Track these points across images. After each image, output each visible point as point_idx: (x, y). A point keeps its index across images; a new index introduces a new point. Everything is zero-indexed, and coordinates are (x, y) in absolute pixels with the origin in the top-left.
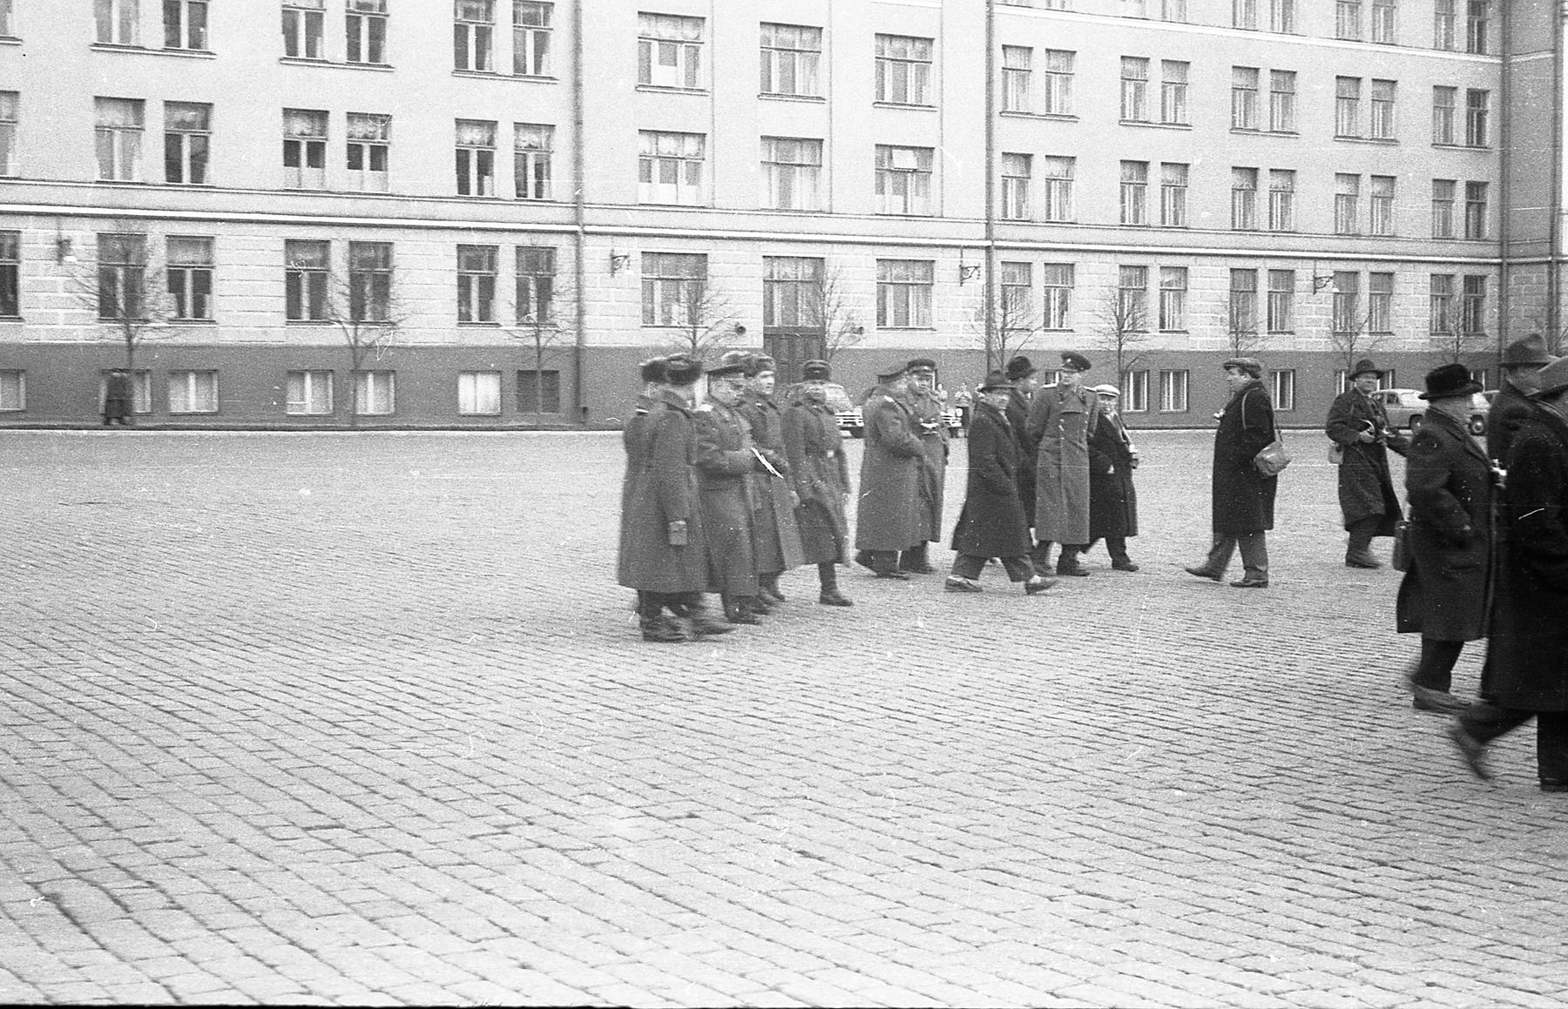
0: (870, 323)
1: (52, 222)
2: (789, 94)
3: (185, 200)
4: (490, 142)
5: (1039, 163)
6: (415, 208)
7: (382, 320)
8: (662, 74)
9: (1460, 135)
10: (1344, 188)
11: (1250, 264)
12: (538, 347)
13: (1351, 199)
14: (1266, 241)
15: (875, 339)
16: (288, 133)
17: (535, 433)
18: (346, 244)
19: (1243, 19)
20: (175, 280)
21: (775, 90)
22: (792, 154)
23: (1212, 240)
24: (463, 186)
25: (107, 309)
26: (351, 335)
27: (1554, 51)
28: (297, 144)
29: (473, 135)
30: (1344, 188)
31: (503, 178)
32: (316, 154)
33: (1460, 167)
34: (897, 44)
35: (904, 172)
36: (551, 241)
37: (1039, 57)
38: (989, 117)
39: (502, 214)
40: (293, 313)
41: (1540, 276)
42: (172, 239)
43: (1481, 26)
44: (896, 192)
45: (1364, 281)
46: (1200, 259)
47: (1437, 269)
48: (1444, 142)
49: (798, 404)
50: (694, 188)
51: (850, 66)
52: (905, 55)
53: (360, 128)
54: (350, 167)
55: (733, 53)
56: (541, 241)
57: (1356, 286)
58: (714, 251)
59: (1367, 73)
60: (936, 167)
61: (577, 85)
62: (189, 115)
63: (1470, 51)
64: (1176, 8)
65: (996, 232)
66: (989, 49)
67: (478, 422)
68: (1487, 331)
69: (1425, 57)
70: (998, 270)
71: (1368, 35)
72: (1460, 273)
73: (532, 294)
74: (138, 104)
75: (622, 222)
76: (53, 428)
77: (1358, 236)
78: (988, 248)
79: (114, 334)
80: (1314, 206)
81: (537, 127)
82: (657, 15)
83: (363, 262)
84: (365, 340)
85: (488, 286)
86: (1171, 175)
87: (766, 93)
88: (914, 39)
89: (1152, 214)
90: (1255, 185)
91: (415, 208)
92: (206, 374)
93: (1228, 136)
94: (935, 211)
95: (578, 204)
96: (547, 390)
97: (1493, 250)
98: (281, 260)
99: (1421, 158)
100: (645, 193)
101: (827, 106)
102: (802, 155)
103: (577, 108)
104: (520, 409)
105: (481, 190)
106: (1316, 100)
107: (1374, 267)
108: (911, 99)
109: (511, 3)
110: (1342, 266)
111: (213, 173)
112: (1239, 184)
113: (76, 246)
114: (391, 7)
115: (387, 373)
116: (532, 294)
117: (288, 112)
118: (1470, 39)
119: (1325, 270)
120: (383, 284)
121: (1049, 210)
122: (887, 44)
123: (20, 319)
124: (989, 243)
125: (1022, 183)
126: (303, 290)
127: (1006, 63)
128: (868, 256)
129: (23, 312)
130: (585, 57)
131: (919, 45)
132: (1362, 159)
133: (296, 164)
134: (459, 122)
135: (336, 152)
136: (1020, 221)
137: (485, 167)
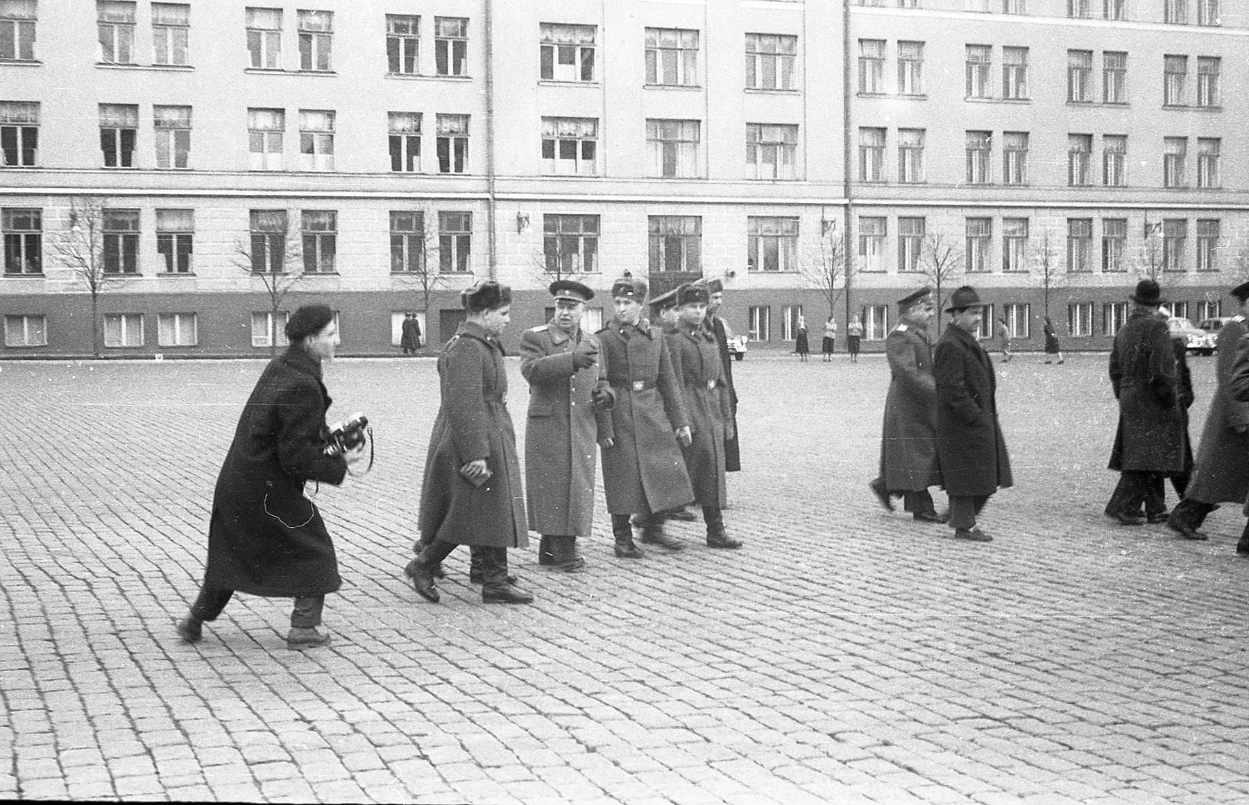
0: (741, 266)
2: (671, 83)
4: (418, 130)
7: (329, 269)
8: (562, 71)
10: (1173, 149)
12: (426, 292)
13: (1180, 158)
14: (1003, 193)
15: (745, 280)
16: (439, 132)
19: (1174, 11)
20: (164, 244)
21: (660, 81)
22: (669, 134)
24: (396, 165)
25: (257, 267)
26: (270, 285)
29: (401, 124)
30: (1173, 149)
31: (428, 157)
34: (766, 41)
35: (774, 145)
36: (466, 206)
37: (892, 46)
38: (846, 98)
39: (427, 182)
42: (160, 212)
45: (1192, 226)
46: (1053, 212)
51: (723, 62)
52: (771, 50)
53: (447, 125)
57: (1185, 232)
60: (800, 140)
61: (488, 83)
64: (1117, 2)
74: (883, 130)
76: (115, 358)
77: (1185, 189)
78: (846, 206)
79: (260, 285)
80: (1144, 163)
81: (456, 117)
83: (315, 226)
84: (280, 288)
86: (1014, 141)
87: (751, 87)
88: (780, 36)
89: (1190, 178)
90: (1090, 147)
92: (187, 316)
94: (799, 174)
95: (490, 176)
98: (247, 225)
100: (256, 161)
101: (702, 94)
102: (687, 133)
103: (489, 101)
105: (410, 167)
106: (1145, 77)
107: (1104, 214)
108: (779, 86)
109: (89, 10)
110: (1173, 215)
111: (40, 156)
112: (1076, 147)
115: (40, 318)
117: (103, 106)
119: (1155, 218)
120: (330, 245)
121: (1200, 180)
123: (43, 276)
124: (847, 201)
125: (879, 151)
126: (266, 248)
127: (864, 57)
128: (959, 217)
129: (45, 270)
130: (495, 63)
131: (786, 42)
134: (391, 114)
136: (879, 181)
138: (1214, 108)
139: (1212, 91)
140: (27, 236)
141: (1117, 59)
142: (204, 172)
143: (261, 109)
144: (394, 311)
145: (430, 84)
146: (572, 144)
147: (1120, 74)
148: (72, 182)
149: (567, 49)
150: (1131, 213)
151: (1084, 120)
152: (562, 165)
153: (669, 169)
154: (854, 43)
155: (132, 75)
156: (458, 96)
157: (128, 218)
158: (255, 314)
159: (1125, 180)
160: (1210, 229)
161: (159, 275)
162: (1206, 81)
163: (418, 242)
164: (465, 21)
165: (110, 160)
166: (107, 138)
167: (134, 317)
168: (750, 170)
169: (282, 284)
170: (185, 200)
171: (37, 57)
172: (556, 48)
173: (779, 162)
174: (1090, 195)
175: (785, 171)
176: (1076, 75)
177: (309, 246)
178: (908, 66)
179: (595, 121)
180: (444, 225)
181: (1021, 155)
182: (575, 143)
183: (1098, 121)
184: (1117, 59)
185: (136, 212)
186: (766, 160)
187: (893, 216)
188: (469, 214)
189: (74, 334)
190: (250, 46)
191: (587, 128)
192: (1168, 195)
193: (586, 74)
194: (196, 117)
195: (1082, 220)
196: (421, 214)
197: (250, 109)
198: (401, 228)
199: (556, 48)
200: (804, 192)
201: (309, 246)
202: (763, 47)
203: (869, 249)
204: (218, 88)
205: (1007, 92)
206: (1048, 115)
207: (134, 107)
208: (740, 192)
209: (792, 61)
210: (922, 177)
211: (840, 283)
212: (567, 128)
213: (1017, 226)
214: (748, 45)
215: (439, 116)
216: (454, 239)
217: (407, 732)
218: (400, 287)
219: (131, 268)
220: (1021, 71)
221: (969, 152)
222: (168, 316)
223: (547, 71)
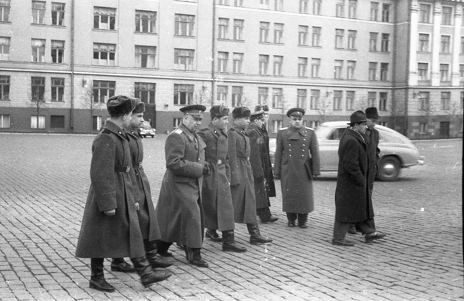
1: (202, 82)
5: (231, 56)
6: (17, 65)
7: (7, 98)
8: (102, 25)
9: (379, 47)
10: (338, 64)
11: (341, 89)
14: (346, 82)
16: (52, 47)
17: (33, 134)
19: (303, 9)
23: (328, 82)
25: (34, 99)
27: (408, 21)
28: (56, 50)
30: (338, 64)
33: (379, 59)
34: (183, 17)
35: (186, 57)
36: (42, 75)
39: (49, 69)
41: (403, 92)
43: (388, 13)
44: (182, 63)
47: (369, 90)
48: (373, 50)
49: (232, 130)
50: (97, 60)
52: (184, 21)
54: (94, 58)
55: (126, 19)
59: (346, 28)
61: (72, 29)
63: (383, 21)
66: (214, 19)
67: (38, 130)
68: (65, 100)
69: (366, 22)
70: (216, 88)
71: (347, 16)
72: (378, 92)
73: (99, 94)
74: (227, 53)
77: (342, 79)
78: (212, 81)
82: (141, 11)
88: (189, 15)
93: (258, 44)
94: (195, 69)
95: (72, 65)
96: (60, 122)
97: (390, 84)
99: (364, 56)
102: (149, 52)
104: (51, 127)
106: (327, 37)
113: (88, 82)
116: (99, 94)
118: (383, 17)
122: (179, 17)
124: (212, 80)
125: (226, 60)
128: (30, 75)
131: (191, 18)
132: (346, 55)
133: (98, 58)
137: (61, 53)
138: (354, 50)
139: (353, 43)
141: (317, 29)
143: (237, 53)
145: (310, 49)
146: (104, 53)
147: (319, 35)
148: (327, 82)
149: (146, 21)
150: (357, 89)
151: (265, 50)
152: (101, 62)
153: (144, 65)
154: (217, 19)
155: (45, 28)
156: (61, 34)
159: (282, 73)
160: (351, 94)
162: (351, 39)
163: (42, 90)
164: (64, 4)
165: (54, 61)
168: (176, 66)
169: (41, 106)
172: (100, 17)
173: (187, 63)
174: (306, 80)
175: (189, 67)
176: (302, 35)
177: (54, 91)
178: (238, 29)
179: (115, 45)
180: (54, 83)
181: (280, 64)
182: (107, 53)
183: (310, 53)
184: (317, 29)
186: (182, 63)
187: (230, 85)
188: (63, 79)
189: (19, 122)
191: (111, 48)
192: (336, 82)
193: (112, 27)
195: (150, 83)
197: (32, 39)
198: (55, 84)
199: (100, 17)
200: (195, 75)
201: (54, 91)
202: (182, 19)
203: (221, 98)
205: (275, 41)
206: (291, 50)
209: (193, 25)
210: (242, 71)
212: (103, 47)
213: (278, 91)
214: (176, 18)
215: (52, 41)
216: (57, 88)
217: (13, 272)
220: (281, 33)
221: (261, 62)
223: (96, 25)
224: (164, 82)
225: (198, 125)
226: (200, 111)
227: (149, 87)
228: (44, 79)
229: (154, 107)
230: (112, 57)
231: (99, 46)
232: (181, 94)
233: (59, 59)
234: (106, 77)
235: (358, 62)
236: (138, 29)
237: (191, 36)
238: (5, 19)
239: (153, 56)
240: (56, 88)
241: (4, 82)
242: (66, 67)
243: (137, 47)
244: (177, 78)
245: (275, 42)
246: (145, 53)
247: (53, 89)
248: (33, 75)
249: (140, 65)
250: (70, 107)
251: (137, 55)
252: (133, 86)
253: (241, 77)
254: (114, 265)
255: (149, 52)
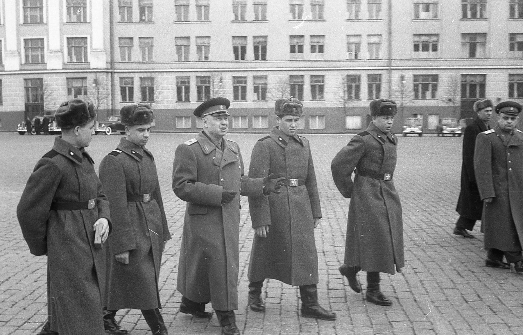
3: (260, 65)
6: (332, 64)
7: (322, 99)
18: (309, 76)
20: (256, 89)
29: (353, 40)
31: (250, 53)
32: (301, 50)
36: (380, 72)
40: (179, 98)
42: (255, 77)
54: (415, 51)
56: (185, 75)
58: (45, 77)
62: (261, 40)
65: (117, 66)
74: (188, 38)
75: (130, 68)
78: (111, 72)
85: (358, 88)
91: (332, 64)
94: (439, 56)
95: (390, 60)
102: (479, 39)
111: (268, 57)
114: (155, 3)
115: (245, 117)
120: (322, 89)
124: (110, 71)
135: (307, 48)
140: (185, 87)
142: (159, 63)
144: (347, 115)
152: (423, 54)
153: (472, 54)
155: (360, 23)
157: (243, 80)
158: (178, 117)
161: (254, 101)
165: (237, 58)
166: (236, 49)
167: (244, 117)
170: (260, 72)
171: (267, 19)
179: (437, 35)
183: (194, 30)
185: (245, 77)
188: (380, 75)
190: (291, 11)
191: (434, 38)
194: (269, 39)
196: (359, 76)
204: (337, 27)
207: (245, 37)
208: (505, 64)
209: (437, 7)
211: (110, 108)
212: (424, 38)
218: (179, 107)
219: (244, 98)
222: (257, 117)
224: (497, 72)
225: (223, 125)
226: (221, 106)
227: (478, 80)
228: (188, 78)
229: (43, 106)
230: (435, 49)
231: (420, 38)
232: (298, 88)
233: (242, 57)
234: (425, 71)
235: (212, 38)
236: (465, 16)
237: (150, 21)
238: (128, 19)
239: (484, 44)
240: (238, 87)
241: (318, 81)
242: (382, 63)
243: (464, 35)
244: (263, 69)
245: (142, 21)
246: (473, 42)
247: (370, 87)
248: (236, 74)
249: (467, 56)
250: (110, 108)
251: (463, 44)
252: (507, 79)
253: (486, 62)
254: (253, 289)
255: (479, 39)
